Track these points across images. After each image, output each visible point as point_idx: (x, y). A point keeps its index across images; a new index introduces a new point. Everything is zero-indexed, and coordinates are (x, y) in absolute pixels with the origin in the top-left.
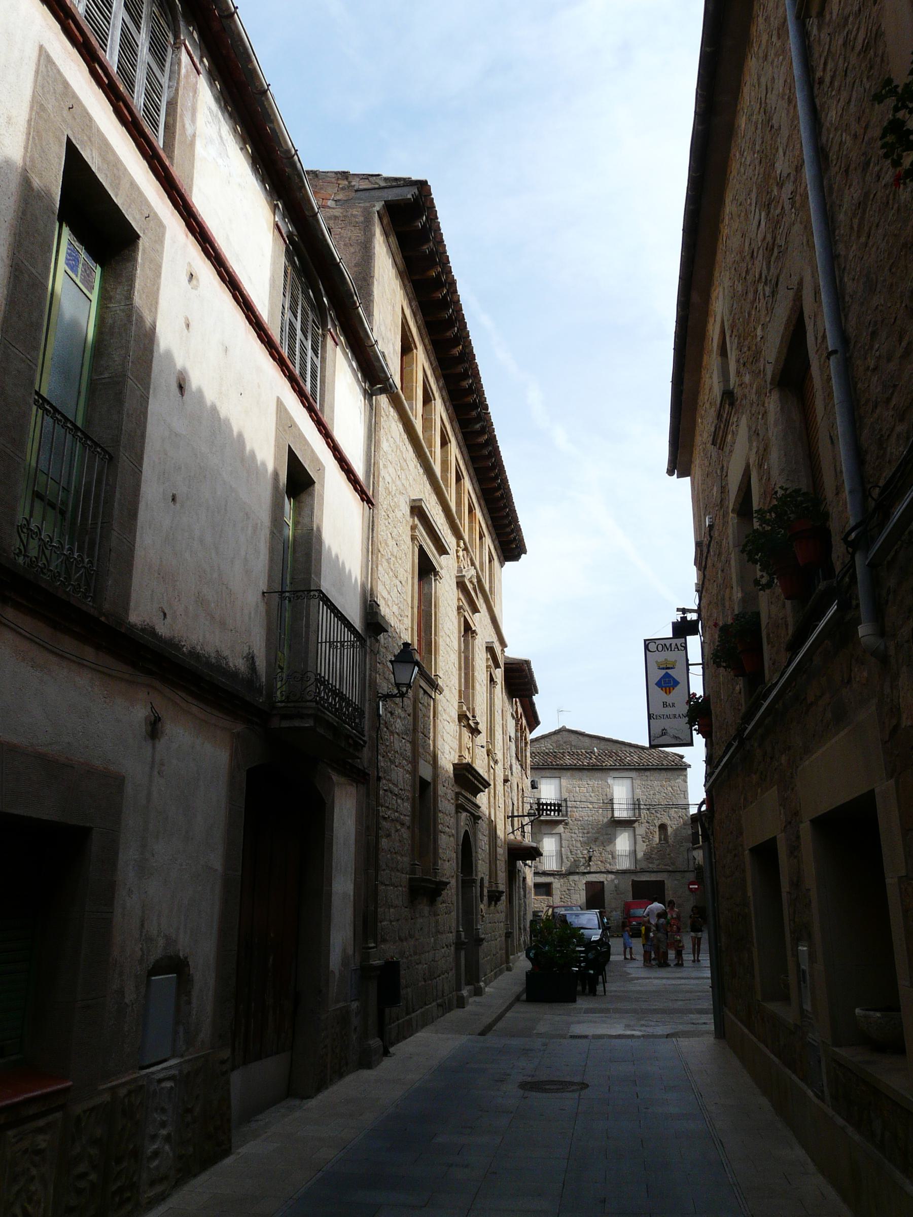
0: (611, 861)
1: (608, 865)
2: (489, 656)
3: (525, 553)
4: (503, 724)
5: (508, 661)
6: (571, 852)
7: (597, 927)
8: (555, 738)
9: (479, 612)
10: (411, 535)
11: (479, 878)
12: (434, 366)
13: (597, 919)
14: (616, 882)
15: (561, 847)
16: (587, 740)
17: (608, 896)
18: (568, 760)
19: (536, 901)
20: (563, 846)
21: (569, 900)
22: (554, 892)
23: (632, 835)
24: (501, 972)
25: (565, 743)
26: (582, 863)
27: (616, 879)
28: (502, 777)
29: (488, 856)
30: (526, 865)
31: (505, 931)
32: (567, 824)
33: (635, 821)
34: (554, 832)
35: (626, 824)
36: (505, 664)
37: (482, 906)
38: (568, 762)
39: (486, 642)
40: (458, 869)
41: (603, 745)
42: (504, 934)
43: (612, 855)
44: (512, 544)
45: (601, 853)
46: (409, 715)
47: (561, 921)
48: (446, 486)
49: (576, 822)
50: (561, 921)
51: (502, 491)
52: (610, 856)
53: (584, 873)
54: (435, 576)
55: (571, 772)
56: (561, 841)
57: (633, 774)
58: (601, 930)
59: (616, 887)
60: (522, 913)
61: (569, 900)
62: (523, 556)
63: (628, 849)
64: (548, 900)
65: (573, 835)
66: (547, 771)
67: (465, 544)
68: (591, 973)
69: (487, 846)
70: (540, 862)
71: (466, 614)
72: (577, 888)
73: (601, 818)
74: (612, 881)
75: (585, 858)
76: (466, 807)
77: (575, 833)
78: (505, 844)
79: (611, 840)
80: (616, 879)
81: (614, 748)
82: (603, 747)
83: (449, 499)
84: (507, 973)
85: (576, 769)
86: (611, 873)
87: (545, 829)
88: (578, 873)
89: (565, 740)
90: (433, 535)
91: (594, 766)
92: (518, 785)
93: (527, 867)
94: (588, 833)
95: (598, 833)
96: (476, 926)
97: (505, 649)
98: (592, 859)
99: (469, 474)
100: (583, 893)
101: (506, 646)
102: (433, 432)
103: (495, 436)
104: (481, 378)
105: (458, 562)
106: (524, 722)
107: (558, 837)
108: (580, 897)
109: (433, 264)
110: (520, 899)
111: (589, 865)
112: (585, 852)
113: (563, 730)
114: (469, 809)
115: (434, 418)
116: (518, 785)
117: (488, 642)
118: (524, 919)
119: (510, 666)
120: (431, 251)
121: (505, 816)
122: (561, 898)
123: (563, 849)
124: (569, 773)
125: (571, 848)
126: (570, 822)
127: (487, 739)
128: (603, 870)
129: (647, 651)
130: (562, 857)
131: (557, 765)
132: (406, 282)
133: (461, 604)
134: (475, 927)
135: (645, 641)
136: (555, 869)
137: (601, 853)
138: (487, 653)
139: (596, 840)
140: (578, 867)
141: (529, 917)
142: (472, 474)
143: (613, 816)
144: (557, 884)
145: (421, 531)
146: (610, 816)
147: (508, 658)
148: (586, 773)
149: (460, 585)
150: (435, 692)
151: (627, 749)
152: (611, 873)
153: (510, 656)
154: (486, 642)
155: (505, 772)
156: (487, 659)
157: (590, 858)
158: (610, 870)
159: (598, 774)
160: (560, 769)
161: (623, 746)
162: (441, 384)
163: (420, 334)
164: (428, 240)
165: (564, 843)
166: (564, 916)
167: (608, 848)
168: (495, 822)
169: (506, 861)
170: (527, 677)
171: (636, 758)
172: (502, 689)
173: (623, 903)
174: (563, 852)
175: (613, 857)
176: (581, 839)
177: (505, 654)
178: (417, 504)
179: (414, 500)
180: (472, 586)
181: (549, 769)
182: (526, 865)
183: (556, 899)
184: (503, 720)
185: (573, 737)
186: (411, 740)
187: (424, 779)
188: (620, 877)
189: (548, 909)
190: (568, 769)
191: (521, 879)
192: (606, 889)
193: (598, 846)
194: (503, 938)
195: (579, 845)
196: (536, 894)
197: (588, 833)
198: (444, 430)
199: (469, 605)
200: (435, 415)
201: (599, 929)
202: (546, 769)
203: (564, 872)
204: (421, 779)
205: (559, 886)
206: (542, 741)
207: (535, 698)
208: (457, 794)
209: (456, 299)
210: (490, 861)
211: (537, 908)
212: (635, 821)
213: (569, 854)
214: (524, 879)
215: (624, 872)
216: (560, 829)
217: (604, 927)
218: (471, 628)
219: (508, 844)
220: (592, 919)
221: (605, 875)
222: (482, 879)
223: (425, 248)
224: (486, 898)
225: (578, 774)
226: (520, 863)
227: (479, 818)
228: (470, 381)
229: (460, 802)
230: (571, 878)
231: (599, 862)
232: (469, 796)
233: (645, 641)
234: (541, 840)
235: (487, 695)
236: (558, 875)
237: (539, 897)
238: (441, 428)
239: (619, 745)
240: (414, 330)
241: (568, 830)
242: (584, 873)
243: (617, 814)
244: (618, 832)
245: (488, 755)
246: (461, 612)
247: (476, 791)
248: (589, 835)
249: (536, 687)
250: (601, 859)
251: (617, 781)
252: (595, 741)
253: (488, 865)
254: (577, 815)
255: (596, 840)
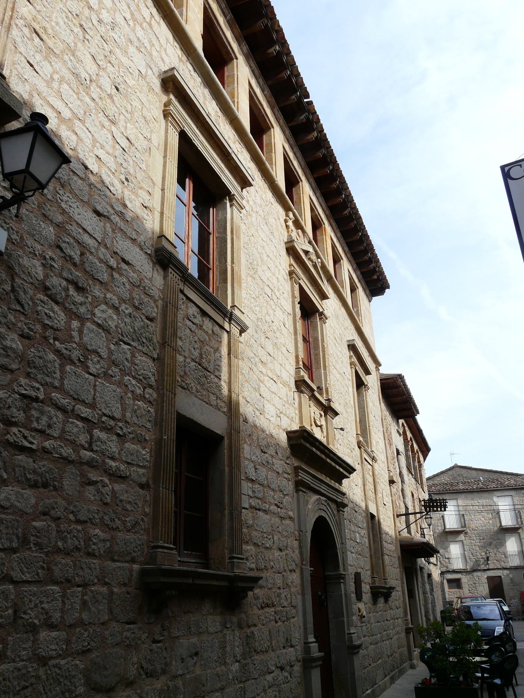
0: (505, 559)
1: (503, 563)
2: (352, 354)
3: (388, 287)
4: (383, 431)
5: (383, 377)
6: (472, 554)
7: (499, 617)
8: (450, 473)
9: (250, 185)
10: (164, 111)
11: (351, 570)
12: (228, 17)
13: (497, 609)
14: (511, 576)
15: (464, 551)
16: (474, 472)
17: (506, 587)
18: (461, 487)
19: (450, 594)
20: (466, 549)
21: (475, 591)
22: (463, 585)
23: (518, 540)
24: (401, 672)
25: (458, 475)
26: (482, 563)
27: (510, 573)
28: (388, 478)
29: (367, 550)
30: (429, 563)
31: (405, 627)
32: (466, 533)
33: (518, 528)
34: (457, 540)
35: (512, 530)
36: (380, 380)
37: (361, 605)
38: (461, 488)
39: (347, 341)
40: (302, 560)
41: (486, 475)
42: (404, 630)
43: (505, 555)
44: (373, 275)
45: (495, 554)
46: (151, 320)
47: (465, 612)
48: (343, 287)
49: (473, 532)
50: (465, 612)
51: (373, 264)
52: (503, 556)
53: (485, 570)
54: (231, 200)
55: (464, 494)
56: (463, 546)
57: (512, 493)
58: (504, 621)
59: (511, 580)
60: (430, 606)
61: (475, 591)
62: (387, 290)
63: (516, 550)
64: (459, 591)
65: (472, 541)
66: (447, 495)
67: (294, 215)
68: (496, 684)
69: (367, 540)
70: (449, 563)
71: (301, 282)
72: (480, 582)
73: (492, 527)
74: (508, 575)
75: (484, 558)
76: (312, 485)
77: (474, 540)
78: (396, 541)
79: (502, 543)
80: (510, 573)
81: (495, 476)
82: (487, 477)
83: (345, 296)
84: (410, 672)
85: (468, 492)
86: (506, 569)
87: (450, 538)
88: (480, 570)
89: (458, 473)
90: (215, 142)
91: (481, 488)
92: (413, 495)
93: (432, 565)
94: (483, 539)
95: (491, 538)
96: (349, 630)
97: (380, 368)
98: (489, 558)
99: (362, 285)
100: (486, 586)
101: (380, 365)
102: (236, 85)
103: (325, 134)
104: (289, 45)
105: (288, 232)
106: (416, 447)
107: (460, 543)
108: (484, 589)
109: (273, 43)
110: (424, 593)
111: (488, 564)
112: (483, 554)
113: (456, 467)
114: (323, 491)
115: (236, 73)
116: (413, 495)
117: (349, 341)
118: (434, 610)
119: (385, 381)
120: (350, 213)
121: (394, 515)
122: (469, 590)
123: (466, 552)
124: (463, 495)
125: (472, 551)
126: (469, 531)
127: (357, 432)
128: (499, 567)
129: (509, 181)
130: (466, 558)
131: (453, 490)
132: (332, 221)
133: (293, 268)
134: (347, 632)
135: (503, 168)
136: (462, 568)
137: (495, 554)
138: (349, 351)
139: (490, 544)
140: (479, 565)
141: (439, 607)
142: (314, 186)
143: (501, 526)
144: (465, 579)
145: (177, 108)
146: (499, 525)
147: (383, 374)
148: (475, 494)
149: (291, 252)
150: (230, 323)
151: (506, 476)
152: (506, 569)
153: (384, 373)
154: (347, 341)
155: (389, 474)
156: (351, 357)
157: (488, 558)
158: (505, 567)
159: (486, 495)
160: (456, 493)
161: (501, 475)
162: (245, 50)
163: (276, 118)
164: (347, 207)
165: (466, 548)
166: (469, 607)
167: (501, 550)
168: (378, 517)
169: (399, 557)
170: (404, 394)
171: (512, 482)
172: (380, 400)
173: (519, 592)
174: (466, 555)
175: (506, 557)
176: (479, 544)
177: (381, 372)
178: (351, 343)
179: (348, 341)
180: (311, 263)
181: (447, 493)
182: (429, 563)
183: (465, 591)
184: (383, 428)
185: (464, 471)
186: (156, 356)
187: (184, 417)
188: (514, 572)
189: (458, 601)
190: (464, 492)
191: (426, 575)
192: (504, 581)
193: (493, 549)
194: (403, 635)
195: (478, 548)
196: (449, 588)
197: (483, 539)
198: (207, 6)
199: (304, 273)
200: (237, 71)
201: (502, 620)
202: (445, 493)
203: (469, 570)
204: (371, 514)
205: (467, 581)
206: (442, 476)
207: (418, 417)
208: (296, 469)
209: (350, 200)
210: (371, 555)
211: (451, 598)
212: (518, 528)
213: (471, 555)
214: (430, 575)
215: (516, 568)
216: (462, 537)
217: (506, 617)
218: (318, 310)
219: (400, 541)
220: (494, 610)
221: (501, 571)
222: (357, 575)
223: (346, 212)
224: (367, 596)
225: (470, 496)
226: (422, 561)
227: (345, 506)
228: (331, 167)
229: (300, 478)
230: (475, 574)
231: (496, 561)
232: (333, 483)
233: (503, 168)
234: (449, 547)
235: (353, 391)
236: (465, 572)
237: (453, 590)
238: (250, 91)
239: (498, 474)
240: (356, 280)
241: (468, 538)
242: (485, 570)
243: (504, 524)
244: (507, 537)
245: (359, 447)
246: (293, 277)
247: (339, 478)
248: (484, 541)
249: (416, 406)
250: (497, 559)
251: (500, 499)
252: (480, 473)
253: (369, 559)
254: (473, 526)
255: (490, 544)
